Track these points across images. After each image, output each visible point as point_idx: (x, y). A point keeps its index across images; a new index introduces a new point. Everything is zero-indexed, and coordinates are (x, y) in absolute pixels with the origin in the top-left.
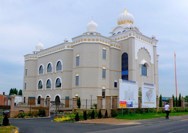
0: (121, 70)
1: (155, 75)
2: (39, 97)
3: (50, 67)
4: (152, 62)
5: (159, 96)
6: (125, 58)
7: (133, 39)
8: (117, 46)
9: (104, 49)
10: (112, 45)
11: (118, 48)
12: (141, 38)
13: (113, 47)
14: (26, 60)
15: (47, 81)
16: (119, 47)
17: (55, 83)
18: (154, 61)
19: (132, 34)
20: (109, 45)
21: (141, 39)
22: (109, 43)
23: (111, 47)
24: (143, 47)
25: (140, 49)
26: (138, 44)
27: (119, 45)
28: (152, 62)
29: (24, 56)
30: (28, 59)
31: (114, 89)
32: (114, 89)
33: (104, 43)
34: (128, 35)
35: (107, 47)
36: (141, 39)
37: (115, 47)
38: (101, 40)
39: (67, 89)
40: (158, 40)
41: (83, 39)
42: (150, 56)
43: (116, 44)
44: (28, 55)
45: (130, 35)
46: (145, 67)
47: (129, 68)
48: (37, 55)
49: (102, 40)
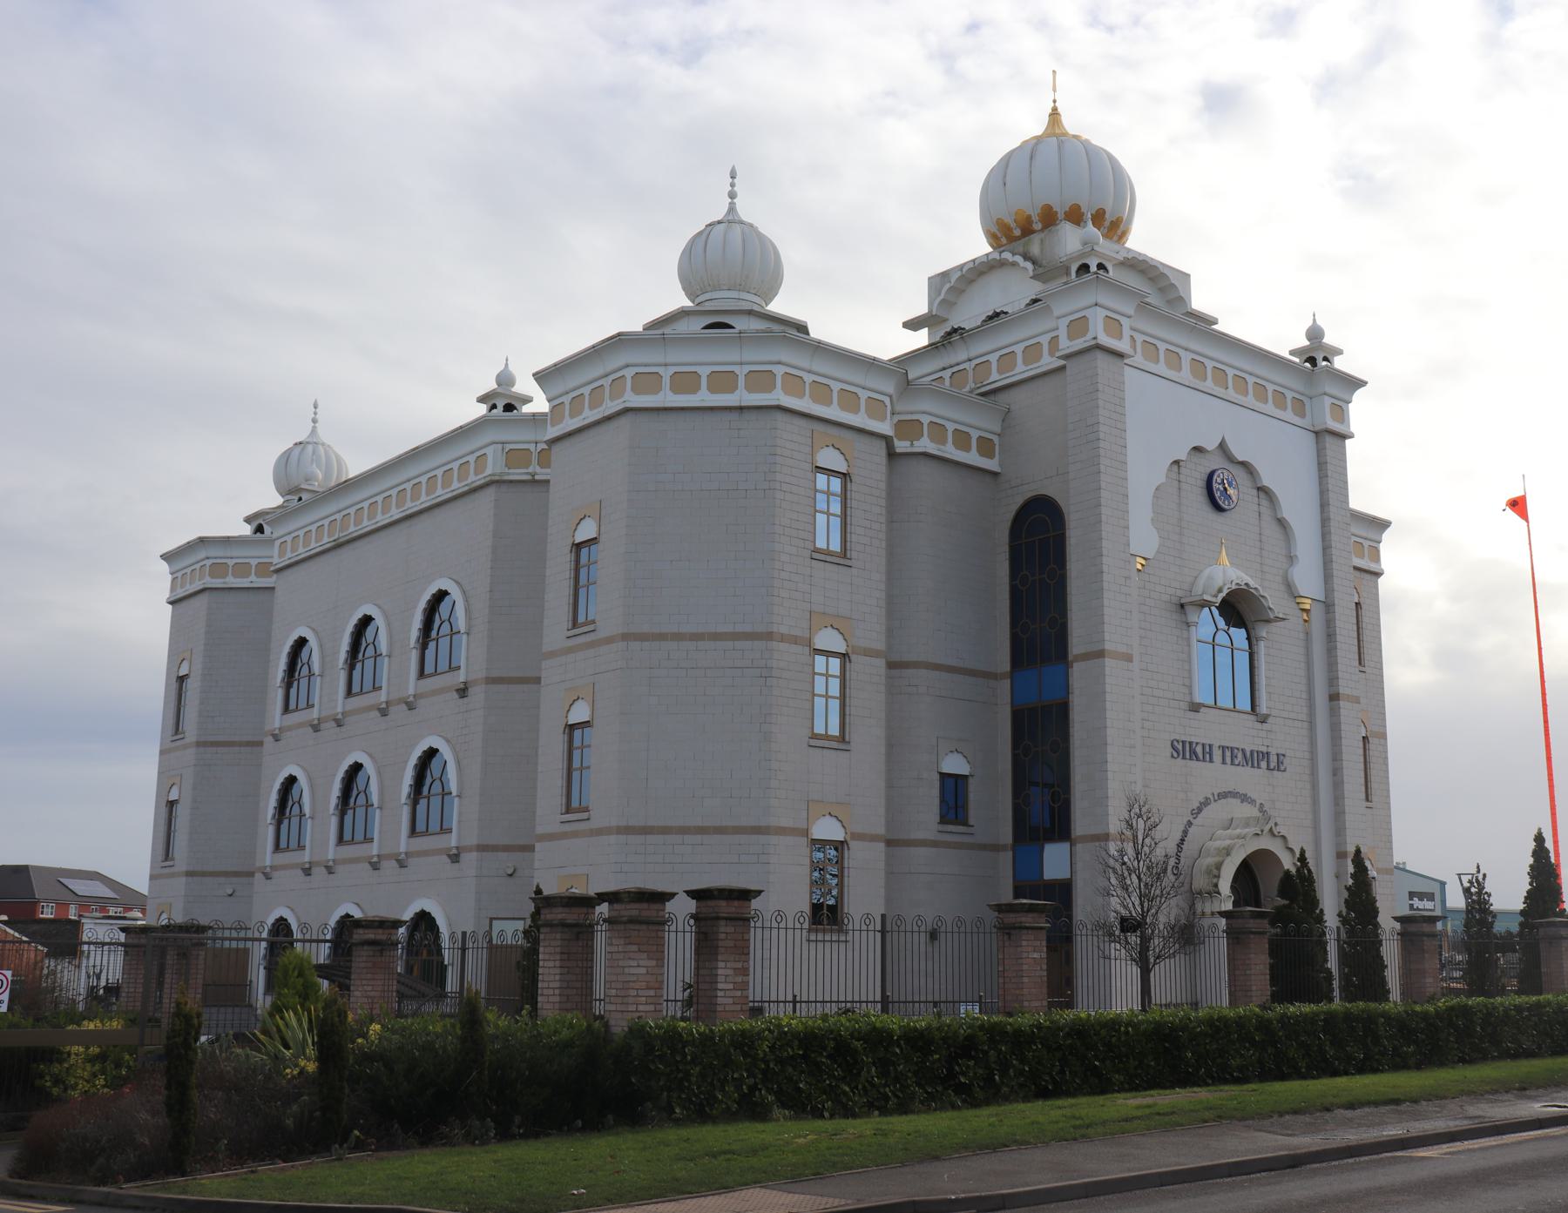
0: (1004, 662)
1: (1334, 697)
2: (281, 926)
3: (445, 629)
4: (1308, 580)
5: (1351, 849)
6: (1039, 545)
7: (1102, 360)
8: (962, 440)
9: (830, 458)
10: (908, 428)
11: (973, 458)
12: (1186, 358)
13: (925, 444)
14: (180, 593)
15: (413, 760)
16: (986, 447)
17: (403, 799)
18: (1328, 577)
19: (1097, 319)
20: (885, 428)
21: (1186, 364)
22: (875, 409)
23: (901, 446)
24: (1211, 444)
25: (1182, 455)
26: (1153, 428)
27: (980, 422)
28: (1308, 580)
29: (168, 557)
30: (217, 588)
31: (935, 844)
32: (935, 844)
33: (833, 412)
34: (1063, 333)
35: (862, 444)
36: (1186, 364)
37: (950, 451)
38: (794, 384)
39: (226, 874)
40: (660, 887)
41: (629, 373)
42: (1282, 523)
43: (955, 416)
44: (202, 541)
45: (1079, 326)
46: (1239, 635)
47: (1077, 644)
48: (272, 541)
49: (808, 378)
